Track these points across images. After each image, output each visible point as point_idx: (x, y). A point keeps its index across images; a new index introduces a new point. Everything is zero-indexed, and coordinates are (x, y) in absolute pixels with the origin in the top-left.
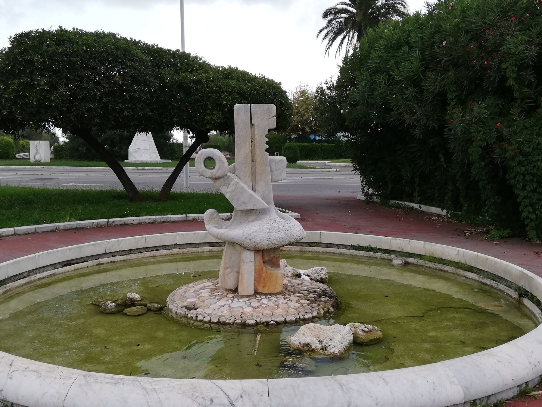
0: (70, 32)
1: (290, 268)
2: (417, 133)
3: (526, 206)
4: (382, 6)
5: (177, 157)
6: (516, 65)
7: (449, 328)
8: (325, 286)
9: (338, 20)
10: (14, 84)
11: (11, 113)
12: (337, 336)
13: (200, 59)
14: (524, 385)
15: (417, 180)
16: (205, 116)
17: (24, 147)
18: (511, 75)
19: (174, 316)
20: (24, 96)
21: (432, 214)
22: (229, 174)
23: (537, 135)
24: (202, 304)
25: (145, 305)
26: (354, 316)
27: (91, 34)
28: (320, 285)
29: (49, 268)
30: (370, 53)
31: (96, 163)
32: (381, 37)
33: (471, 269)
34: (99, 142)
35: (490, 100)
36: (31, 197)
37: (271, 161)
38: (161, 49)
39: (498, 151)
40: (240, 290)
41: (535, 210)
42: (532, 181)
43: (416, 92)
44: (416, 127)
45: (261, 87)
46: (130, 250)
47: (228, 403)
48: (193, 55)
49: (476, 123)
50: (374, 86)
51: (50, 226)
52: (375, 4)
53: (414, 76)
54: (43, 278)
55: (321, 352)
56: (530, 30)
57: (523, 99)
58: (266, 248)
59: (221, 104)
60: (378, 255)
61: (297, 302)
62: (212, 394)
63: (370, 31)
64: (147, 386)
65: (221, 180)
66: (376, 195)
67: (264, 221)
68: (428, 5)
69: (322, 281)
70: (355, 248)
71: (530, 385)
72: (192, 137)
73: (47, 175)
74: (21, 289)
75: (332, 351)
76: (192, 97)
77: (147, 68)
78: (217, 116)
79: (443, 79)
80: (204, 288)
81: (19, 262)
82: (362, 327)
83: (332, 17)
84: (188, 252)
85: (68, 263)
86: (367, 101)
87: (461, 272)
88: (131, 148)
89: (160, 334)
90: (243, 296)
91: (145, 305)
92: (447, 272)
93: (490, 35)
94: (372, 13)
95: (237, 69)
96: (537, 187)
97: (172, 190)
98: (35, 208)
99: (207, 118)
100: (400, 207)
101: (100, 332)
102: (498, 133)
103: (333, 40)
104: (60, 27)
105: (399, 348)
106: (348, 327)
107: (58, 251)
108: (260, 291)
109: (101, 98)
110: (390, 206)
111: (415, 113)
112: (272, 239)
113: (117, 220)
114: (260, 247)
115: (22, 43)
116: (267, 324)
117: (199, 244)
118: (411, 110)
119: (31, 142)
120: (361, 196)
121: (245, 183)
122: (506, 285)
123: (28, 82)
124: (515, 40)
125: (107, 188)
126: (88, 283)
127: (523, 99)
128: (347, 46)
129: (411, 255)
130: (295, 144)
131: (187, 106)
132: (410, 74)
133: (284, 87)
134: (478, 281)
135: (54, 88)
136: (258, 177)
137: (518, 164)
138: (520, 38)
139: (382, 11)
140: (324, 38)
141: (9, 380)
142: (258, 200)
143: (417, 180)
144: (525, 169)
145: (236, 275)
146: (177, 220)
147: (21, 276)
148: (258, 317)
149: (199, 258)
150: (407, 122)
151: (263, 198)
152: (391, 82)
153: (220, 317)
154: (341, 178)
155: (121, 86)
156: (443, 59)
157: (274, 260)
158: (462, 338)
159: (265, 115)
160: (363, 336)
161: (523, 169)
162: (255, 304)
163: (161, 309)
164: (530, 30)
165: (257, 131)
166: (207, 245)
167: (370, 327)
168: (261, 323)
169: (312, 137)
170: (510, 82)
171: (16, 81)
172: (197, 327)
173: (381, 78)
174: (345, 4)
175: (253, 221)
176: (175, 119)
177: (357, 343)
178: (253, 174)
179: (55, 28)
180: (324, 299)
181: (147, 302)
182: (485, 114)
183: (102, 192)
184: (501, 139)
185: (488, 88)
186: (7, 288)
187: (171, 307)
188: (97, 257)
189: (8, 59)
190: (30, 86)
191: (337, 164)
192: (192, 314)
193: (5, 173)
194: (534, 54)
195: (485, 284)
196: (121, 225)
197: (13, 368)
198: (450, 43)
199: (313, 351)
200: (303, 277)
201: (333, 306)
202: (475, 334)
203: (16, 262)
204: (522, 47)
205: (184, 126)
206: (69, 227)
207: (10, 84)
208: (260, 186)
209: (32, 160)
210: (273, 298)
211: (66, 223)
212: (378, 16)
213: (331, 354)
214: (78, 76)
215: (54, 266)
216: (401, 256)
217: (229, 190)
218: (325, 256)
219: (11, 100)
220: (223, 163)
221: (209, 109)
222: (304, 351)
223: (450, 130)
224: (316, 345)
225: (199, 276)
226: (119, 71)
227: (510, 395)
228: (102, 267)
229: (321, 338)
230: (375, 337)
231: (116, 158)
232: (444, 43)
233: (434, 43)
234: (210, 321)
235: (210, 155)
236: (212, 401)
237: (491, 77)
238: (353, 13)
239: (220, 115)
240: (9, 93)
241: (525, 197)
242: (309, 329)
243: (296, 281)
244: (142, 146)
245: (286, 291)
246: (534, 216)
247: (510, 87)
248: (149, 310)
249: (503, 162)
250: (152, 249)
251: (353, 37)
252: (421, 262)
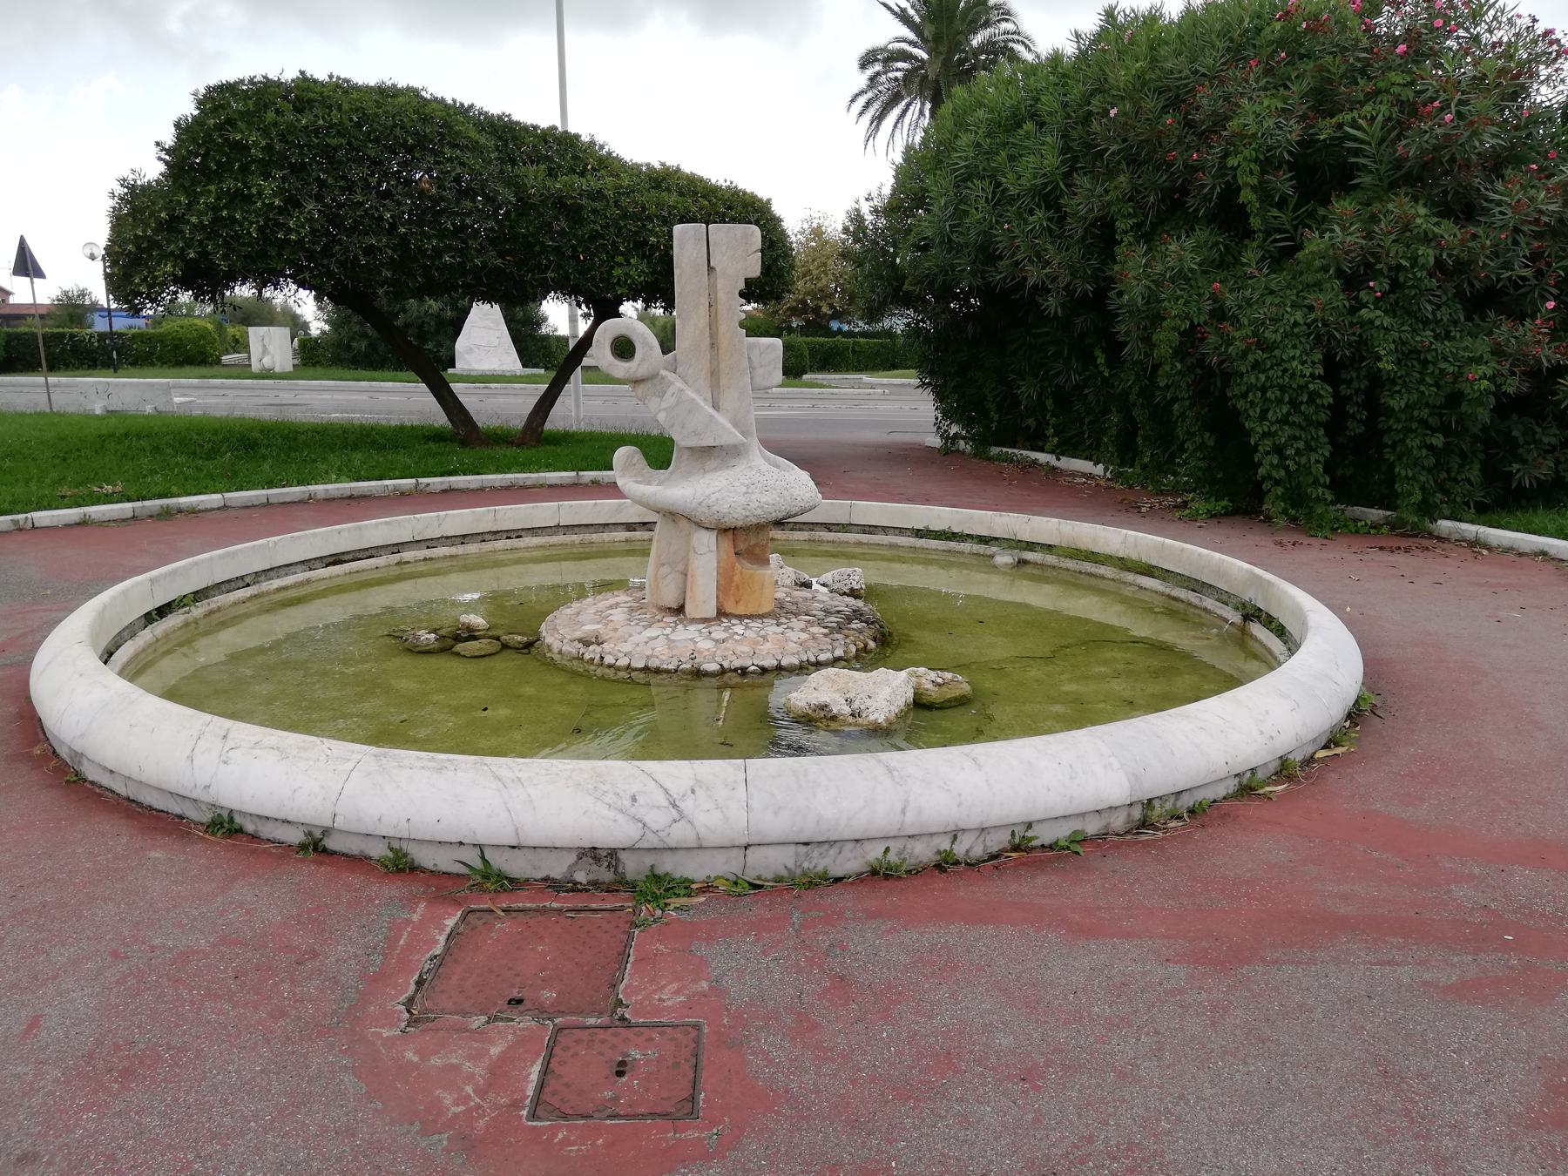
0: (323, 84)
1: (789, 570)
2: (1052, 304)
3: (1268, 453)
4: (982, 48)
5: (557, 362)
6: (1256, 160)
7: (1103, 678)
8: (860, 603)
9: (891, 75)
10: (210, 194)
11: (204, 254)
12: (885, 691)
13: (602, 147)
14: (1248, 775)
15: (1049, 403)
16: (612, 268)
17: (237, 341)
18: (1247, 179)
19: (557, 657)
20: (233, 220)
21: (1074, 474)
22: (664, 373)
23: (1292, 306)
24: (612, 634)
25: (498, 639)
26: (916, 656)
27: (368, 90)
28: (850, 600)
29: (299, 568)
30: (956, 137)
31: (387, 374)
32: (981, 105)
33: (1149, 571)
34: (390, 328)
35: (1202, 234)
36: (256, 434)
37: (751, 347)
38: (518, 123)
39: (1212, 339)
40: (688, 609)
41: (1283, 457)
42: (1280, 401)
43: (1050, 220)
44: (1049, 291)
45: (730, 208)
46: (464, 536)
47: (666, 804)
48: (585, 138)
49: (1172, 280)
50: (963, 207)
51: (295, 491)
52: (968, 42)
53: (1046, 184)
54: (285, 588)
55: (851, 720)
56: (1286, 87)
57: (1268, 234)
58: (740, 524)
59: (646, 242)
60: (966, 547)
61: (802, 630)
62: (635, 787)
63: (959, 91)
64: (503, 773)
65: (648, 385)
66: (964, 438)
67: (737, 469)
68: (1077, 35)
69: (853, 593)
70: (919, 533)
71: (1260, 775)
72: (586, 316)
73: (287, 397)
74: (242, 609)
75: (872, 718)
76: (581, 226)
77: (490, 163)
78: (638, 269)
79: (1107, 191)
80: (617, 605)
81: (234, 554)
82: (932, 675)
83: (878, 67)
84: (583, 542)
85: (336, 560)
86: (950, 240)
87: (1130, 577)
88: (461, 344)
89: (528, 690)
90: (694, 621)
91: (498, 639)
92: (1103, 577)
93: (1206, 99)
94: (961, 62)
95: (678, 169)
96: (1289, 414)
97: (548, 426)
98: (264, 458)
99: (617, 272)
100: (1012, 461)
101: (407, 685)
102: (1215, 301)
103: (879, 118)
105: (1002, 713)
106: (903, 674)
107: (315, 535)
108: (728, 610)
109: (393, 227)
110: (990, 459)
111: (1048, 263)
112: (754, 505)
113: (436, 482)
114: (729, 522)
115: (222, 106)
116: (744, 671)
117: (605, 527)
118: (1039, 256)
119: (251, 329)
120: (935, 441)
121: (697, 391)
122: (1218, 600)
123: (238, 190)
124: (1257, 108)
125: (415, 420)
126: (377, 600)
127: (1268, 234)
128: (911, 125)
129: (1031, 546)
130: (800, 339)
131: (574, 248)
132: (1039, 181)
133: (777, 209)
134: (1162, 594)
135: (293, 203)
136: (724, 381)
137: (1253, 367)
138: (1266, 103)
139: (983, 57)
140: (861, 114)
141: (223, 766)
142: (724, 430)
143: (1049, 403)
144: (1267, 378)
145: (680, 578)
147: (241, 584)
148: (725, 658)
149: (605, 554)
150: (1031, 281)
151: (735, 425)
152: (1000, 199)
153: (648, 657)
154: (900, 406)
155: (436, 201)
156: (1106, 150)
157: (757, 551)
158: (1127, 694)
159: (738, 250)
160: (934, 694)
161: (1262, 377)
162: (718, 632)
163: (529, 645)
164: (1286, 87)
165: (720, 283)
167: (948, 676)
168: (731, 670)
169: (835, 325)
170: (1246, 196)
171: (212, 188)
172: (602, 678)
173: (979, 189)
174: (905, 40)
175: (715, 470)
176: (550, 275)
177: (920, 704)
178: (714, 375)
179: (290, 75)
180: (856, 625)
181: (498, 632)
182: (1192, 262)
183: (402, 428)
184: (1219, 314)
185: (1197, 210)
186: (213, 606)
187: (549, 640)
188: (397, 548)
189: (194, 140)
190: (241, 198)
191: (885, 381)
192: (592, 652)
193: (201, 392)
194: (1294, 137)
195: (1175, 599)
196: (444, 491)
197: (230, 744)
198: (1125, 114)
199: (834, 718)
200: (815, 586)
201: (875, 640)
202: (1153, 688)
203: (228, 554)
204: (1270, 122)
205: (568, 289)
206: (337, 494)
207: (202, 194)
208: (729, 399)
209: (255, 367)
210: (756, 624)
211: (329, 486)
212: (974, 68)
213: (870, 723)
214: (344, 178)
215: (308, 564)
216: (1011, 548)
217: (664, 405)
218: (859, 550)
219: (203, 227)
220: (651, 348)
221: (622, 254)
222: (817, 719)
223: (1120, 294)
224: (840, 707)
225: (604, 587)
226: (429, 171)
227: (1221, 791)
228: (407, 569)
229: (851, 695)
230: (958, 693)
231: (430, 360)
232: (1113, 112)
233: (1090, 113)
234: (628, 667)
235: (624, 332)
236: (634, 799)
237: (1203, 186)
238: (922, 60)
239: (643, 266)
240: (200, 214)
241: (1265, 435)
242: (827, 678)
243: (805, 593)
244: (483, 340)
245: (781, 612)
246: (1282, 473)
247: (1244, 205)
248: (505, 646)
249: (1223, 362)
250: (509, 534)
251: (921, 113)
252: (1051, 559)
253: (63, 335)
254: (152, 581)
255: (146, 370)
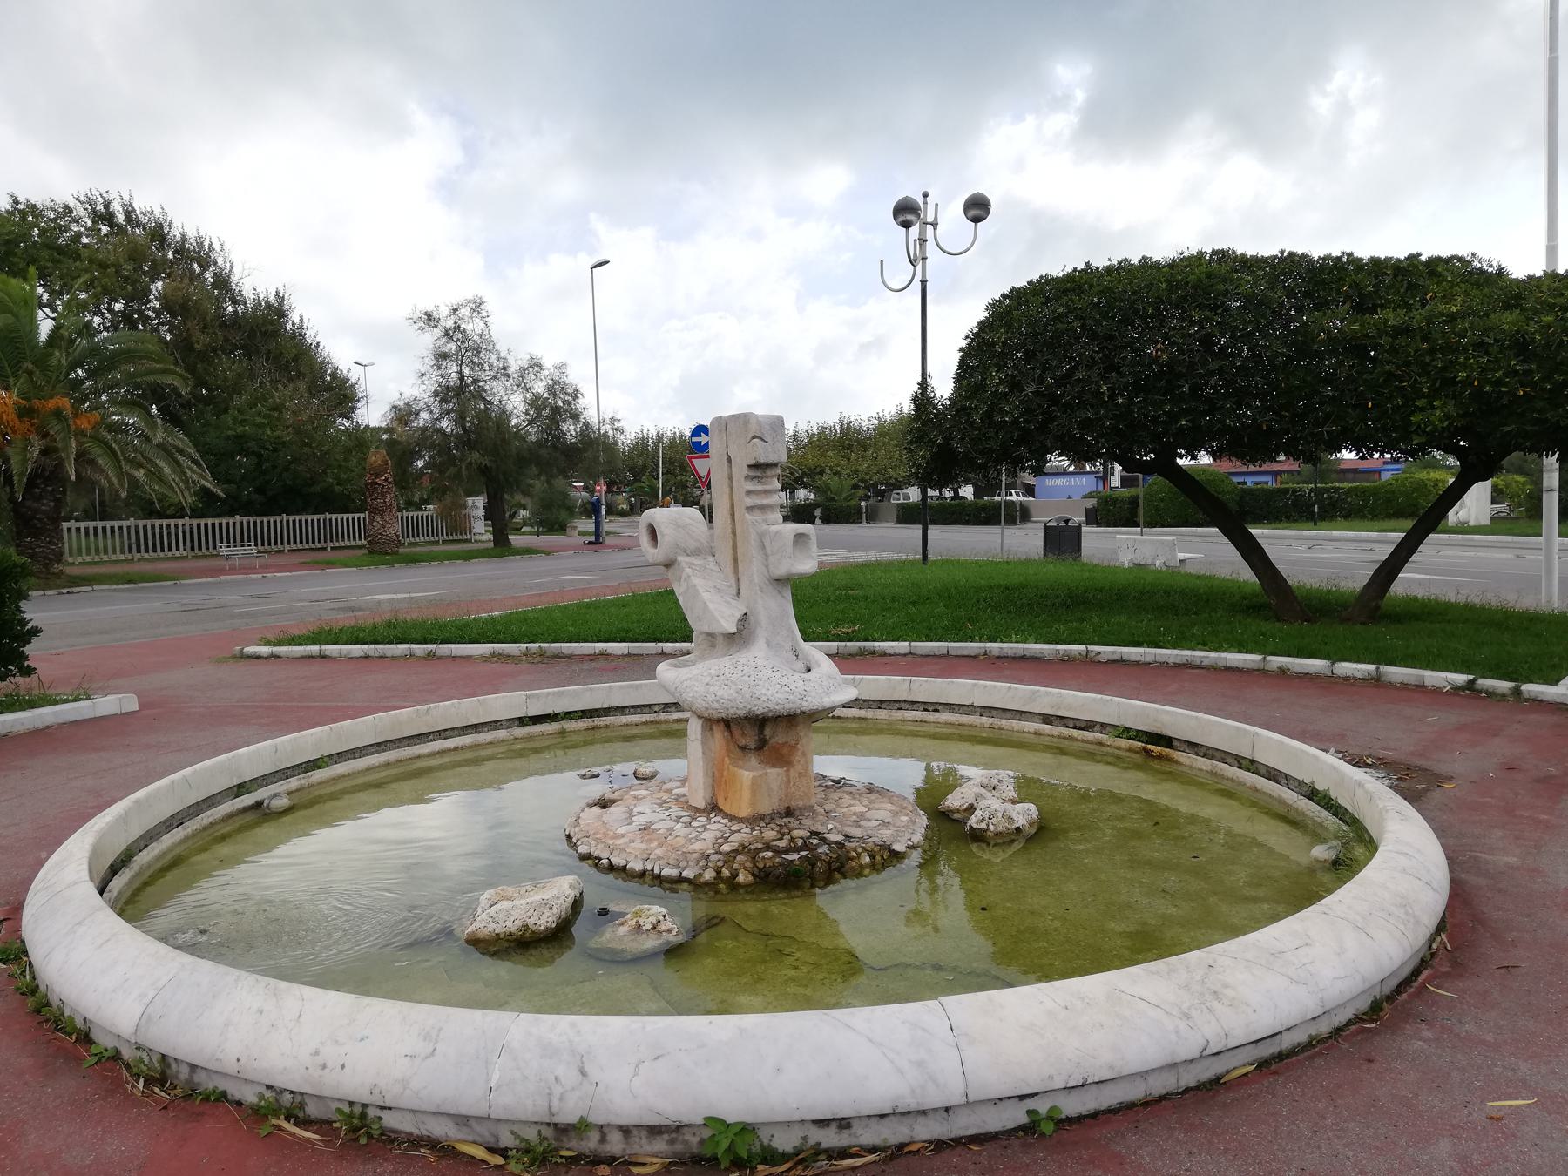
46: (882, 701)
59: (1454, 381)
104: (1087, 264)
112: (711, 698)
117: (1021, 714)
146: (1241, 665)
157: (785, 751)
166: (1037, 718)
193: (1352, 546)
206: (1010, 653)
239: (1451, 408)
250: (927, 706)
253: (1287, 490)
254: (528, 697)
255: (1357, 523)
